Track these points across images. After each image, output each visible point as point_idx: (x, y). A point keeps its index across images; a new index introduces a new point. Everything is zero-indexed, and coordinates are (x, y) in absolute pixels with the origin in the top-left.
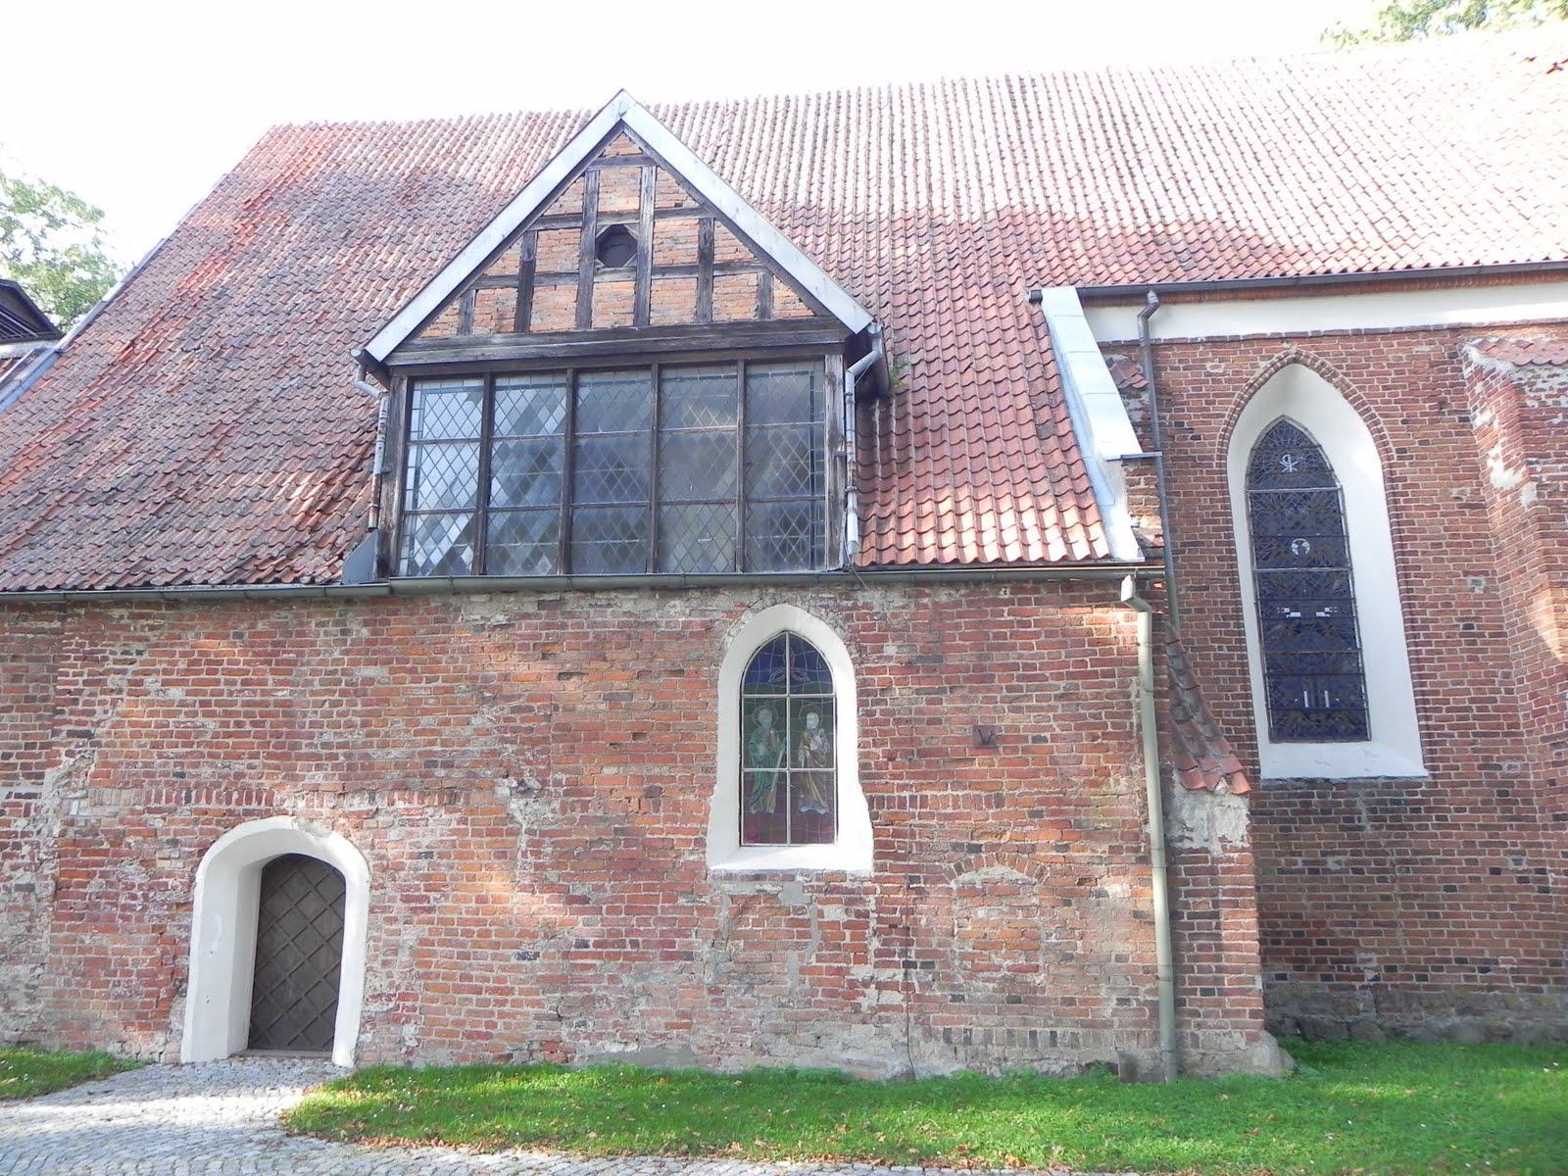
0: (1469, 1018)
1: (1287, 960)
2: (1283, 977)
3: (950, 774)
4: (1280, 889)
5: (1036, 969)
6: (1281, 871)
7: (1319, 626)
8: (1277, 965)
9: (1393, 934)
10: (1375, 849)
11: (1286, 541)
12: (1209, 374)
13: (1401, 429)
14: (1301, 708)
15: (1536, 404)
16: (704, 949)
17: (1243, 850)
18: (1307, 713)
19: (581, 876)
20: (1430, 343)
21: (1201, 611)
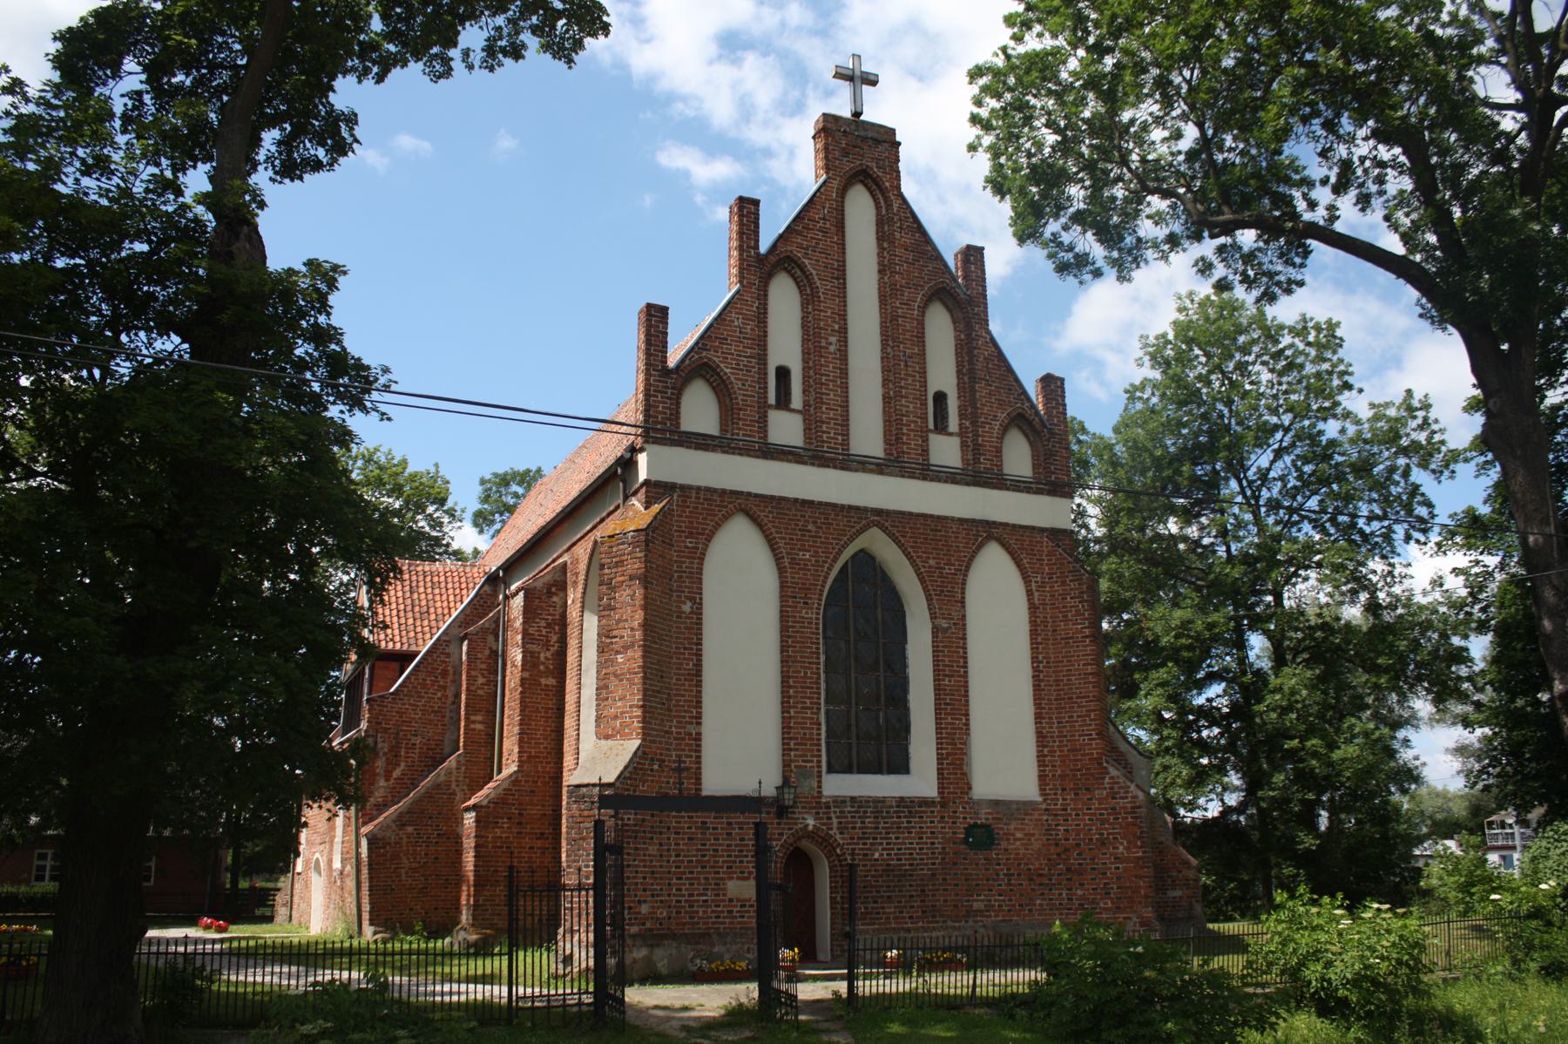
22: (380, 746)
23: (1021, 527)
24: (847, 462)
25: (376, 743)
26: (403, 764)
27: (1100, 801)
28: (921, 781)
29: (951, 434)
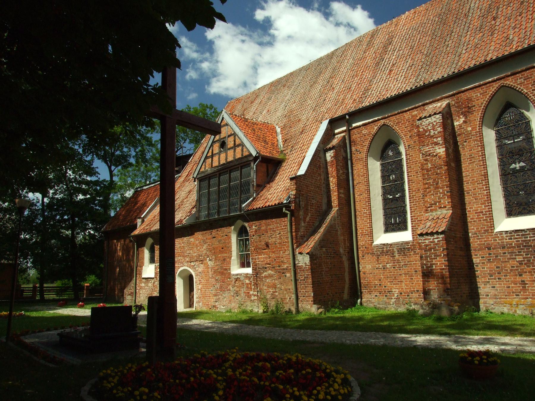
0: (416, 306)
1: (378, 292)
2: (376, 296)
3: (263, 252)
4: (376, 273)
5: (276, 292)
6: (377, 268)
7: (397, 199)
8: (375, 293)
9: (402, 284)
10: (398, 261)
11: (389, 176)
12: (363, 134)
13: (409, 139)
14: (391, 224)
15: (422, 130)
16: (231, 289)
17: (308, 265)
18: (393, 224)
19: (217, 275)
20: (417, 111)
21: (360, 201)
22: (301, 203)
25: (300, 201)
26: (309, 214)
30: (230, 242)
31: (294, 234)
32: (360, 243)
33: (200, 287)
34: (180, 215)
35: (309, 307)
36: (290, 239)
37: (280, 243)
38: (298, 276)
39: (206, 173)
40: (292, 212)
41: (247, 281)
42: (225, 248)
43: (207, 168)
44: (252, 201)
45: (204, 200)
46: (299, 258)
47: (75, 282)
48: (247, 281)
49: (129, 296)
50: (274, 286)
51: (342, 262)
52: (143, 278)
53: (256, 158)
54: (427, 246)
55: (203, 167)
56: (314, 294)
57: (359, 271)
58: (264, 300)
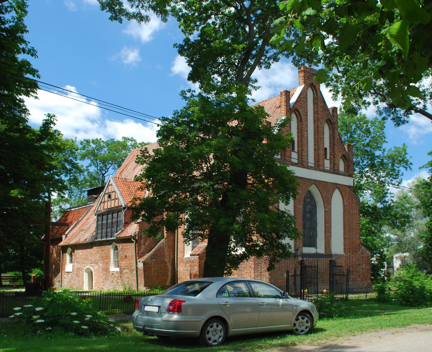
16: (110, 279)
19: (103, 272)
22: (142, 236)
23: (343, 185)
24: (308, 168)
25: (141, 235)
26: (148, 241)
27: (359, 255)
28: (321, 249)
29: (328, 159)
30: (110, 254)
31: (137, 252)
32: (179, 256)
33: (96, 277)
34: (87, 235)
35: (142, 288)
36: (134, 255)
37: (131, 256)
38: (138, 273)
39: (101, 212)
40: (136, 240)
41: (117, 275)
42: (107, 257)
43: (101, 209)
44: (121, 232)
45: (100, 227)
46: (139, 264)
47: (24, 273)
48: (117, 275)
49: (58, 283)
50: (129, 278)
51: (166, 266)
52: (66, 272)
53: (124, 208)
54: (192, 260)
55: (99, 208)
56: (145, 282)
57: (177, 271)
58: (124, 285)
